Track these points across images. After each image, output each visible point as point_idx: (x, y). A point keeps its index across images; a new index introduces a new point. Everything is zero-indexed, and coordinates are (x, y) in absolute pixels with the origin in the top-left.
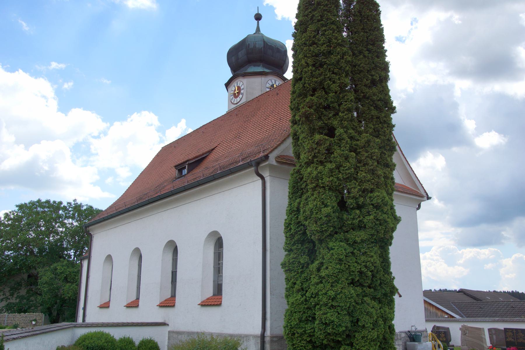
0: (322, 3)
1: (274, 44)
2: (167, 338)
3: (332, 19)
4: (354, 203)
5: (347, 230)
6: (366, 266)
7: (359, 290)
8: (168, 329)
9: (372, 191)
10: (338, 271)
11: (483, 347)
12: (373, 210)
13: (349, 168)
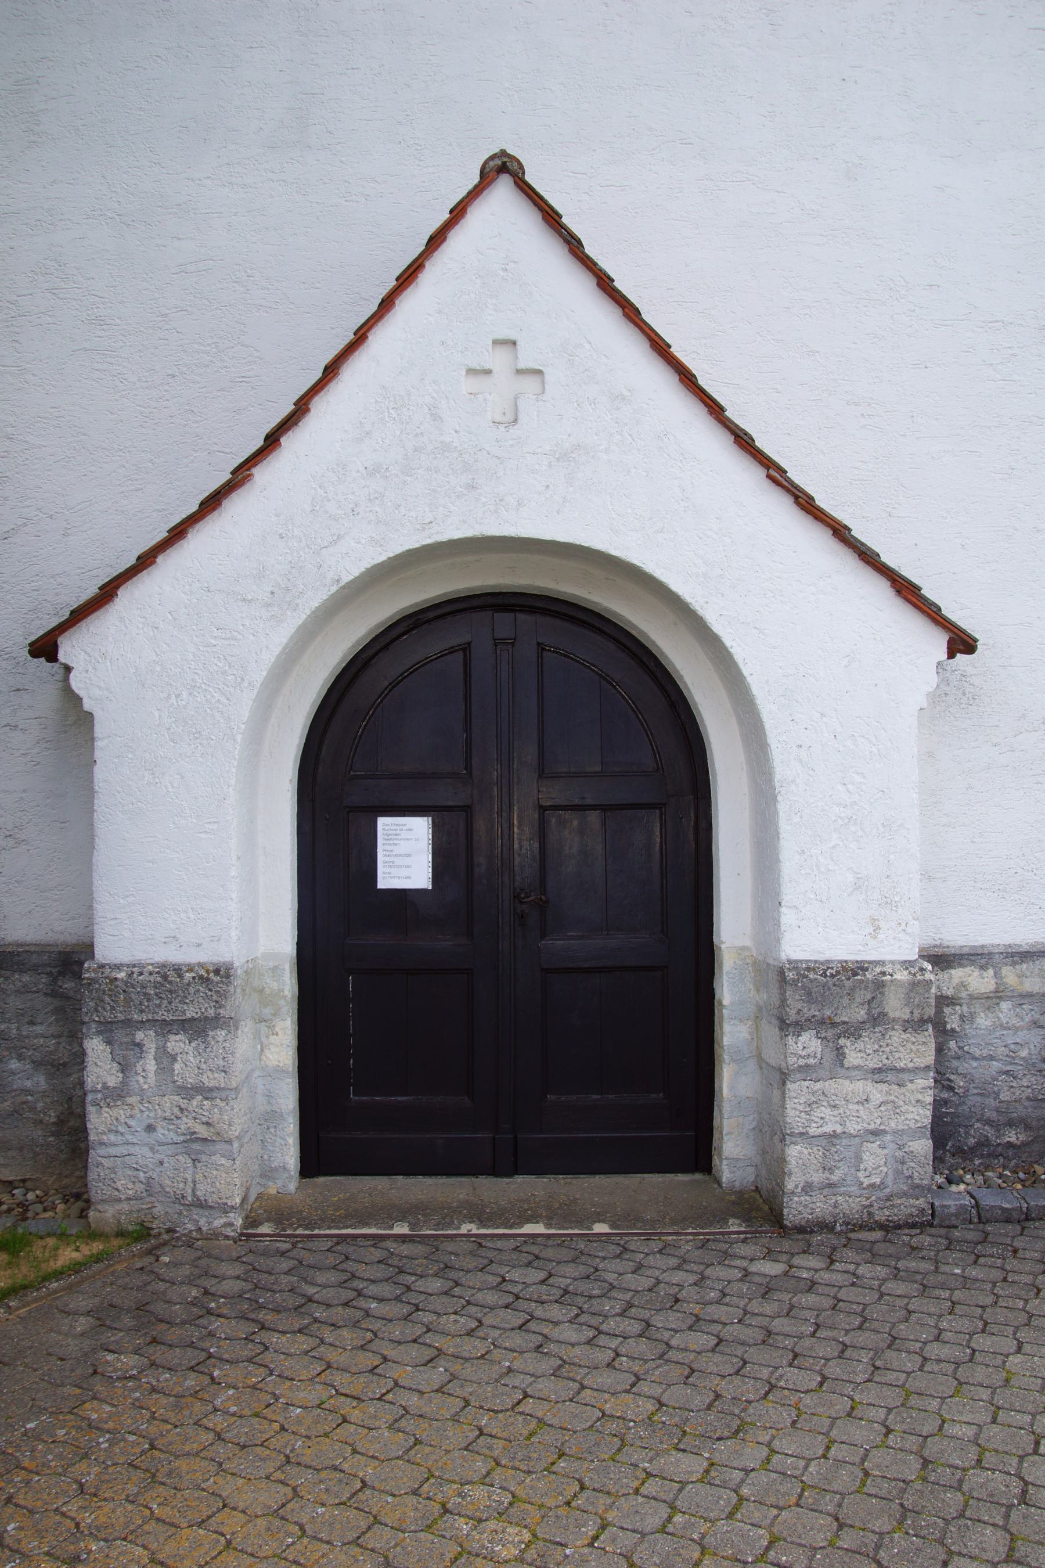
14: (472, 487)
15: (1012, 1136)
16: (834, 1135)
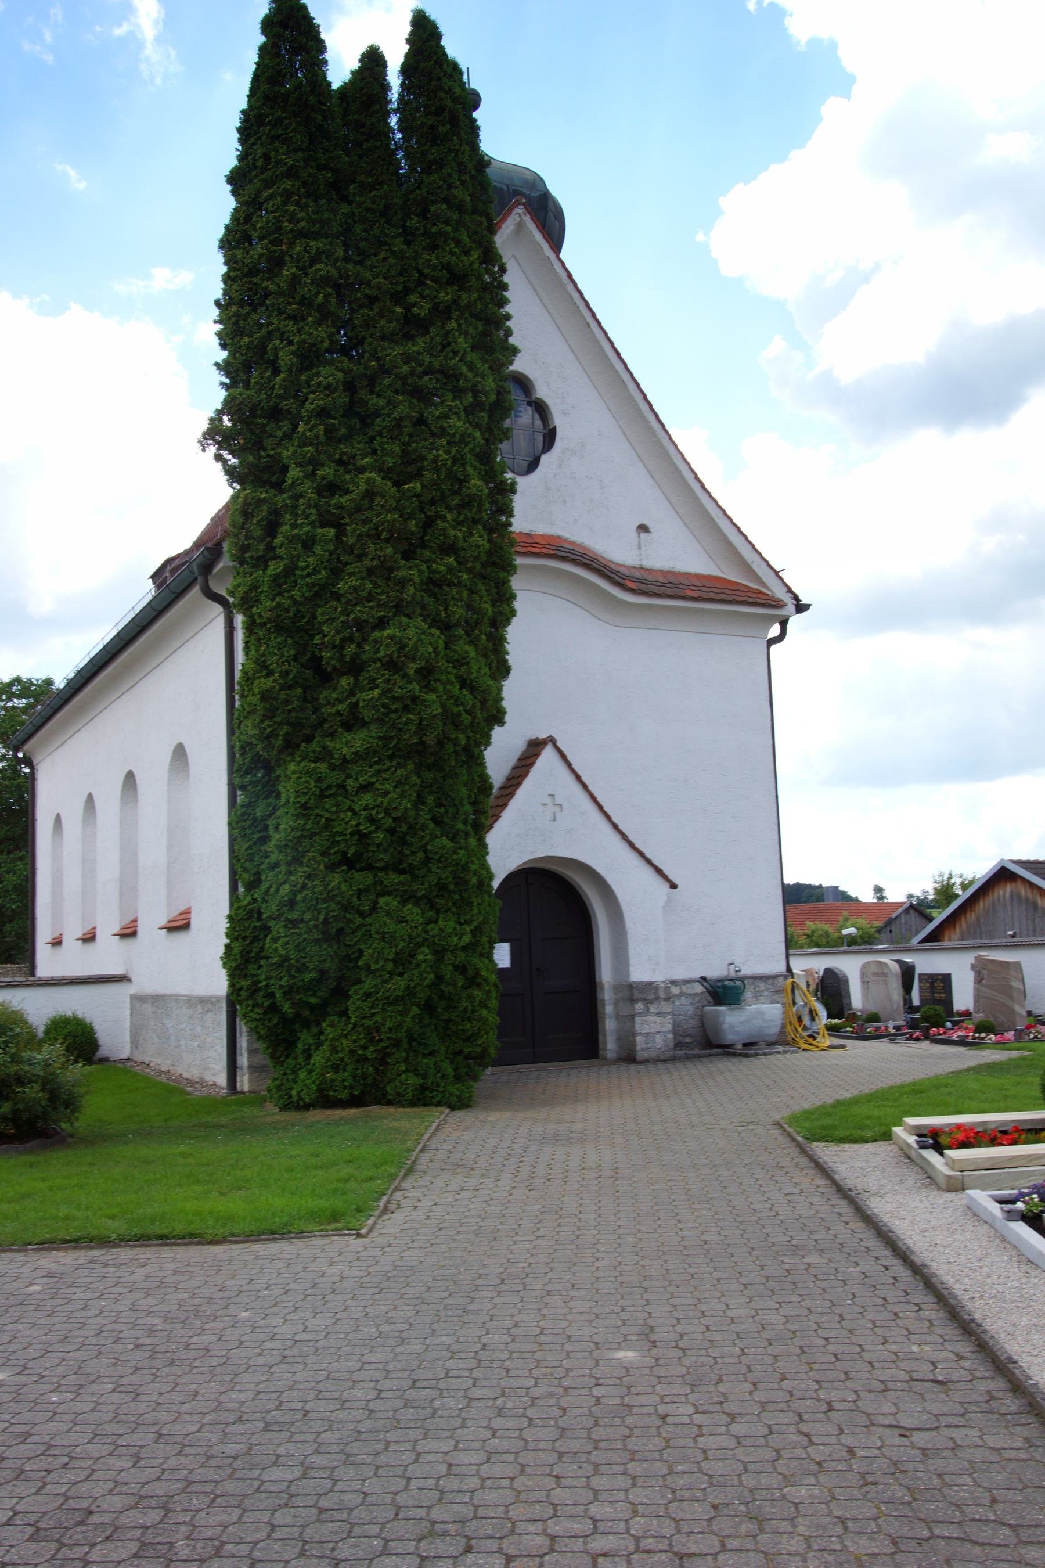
0: (267, 117)
1: (506, 181)
2: (128, 1012)
3: (286, 164)
4: (333, 658)
5: (331, 730)
6: (372, 820)
7: (366, 879)
8: (131, 989)
9: (382, 624)
10: (299, 833)
11: (1013, 1012)
12: (383, 675)
13: (315, 571)
14: (545, 841)
15: (688, 1040)
16: (648, 1033)
